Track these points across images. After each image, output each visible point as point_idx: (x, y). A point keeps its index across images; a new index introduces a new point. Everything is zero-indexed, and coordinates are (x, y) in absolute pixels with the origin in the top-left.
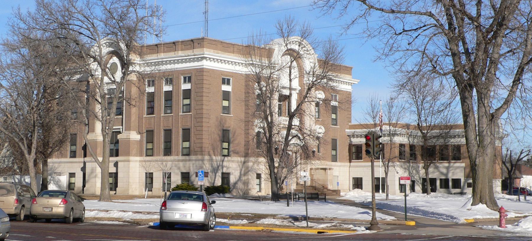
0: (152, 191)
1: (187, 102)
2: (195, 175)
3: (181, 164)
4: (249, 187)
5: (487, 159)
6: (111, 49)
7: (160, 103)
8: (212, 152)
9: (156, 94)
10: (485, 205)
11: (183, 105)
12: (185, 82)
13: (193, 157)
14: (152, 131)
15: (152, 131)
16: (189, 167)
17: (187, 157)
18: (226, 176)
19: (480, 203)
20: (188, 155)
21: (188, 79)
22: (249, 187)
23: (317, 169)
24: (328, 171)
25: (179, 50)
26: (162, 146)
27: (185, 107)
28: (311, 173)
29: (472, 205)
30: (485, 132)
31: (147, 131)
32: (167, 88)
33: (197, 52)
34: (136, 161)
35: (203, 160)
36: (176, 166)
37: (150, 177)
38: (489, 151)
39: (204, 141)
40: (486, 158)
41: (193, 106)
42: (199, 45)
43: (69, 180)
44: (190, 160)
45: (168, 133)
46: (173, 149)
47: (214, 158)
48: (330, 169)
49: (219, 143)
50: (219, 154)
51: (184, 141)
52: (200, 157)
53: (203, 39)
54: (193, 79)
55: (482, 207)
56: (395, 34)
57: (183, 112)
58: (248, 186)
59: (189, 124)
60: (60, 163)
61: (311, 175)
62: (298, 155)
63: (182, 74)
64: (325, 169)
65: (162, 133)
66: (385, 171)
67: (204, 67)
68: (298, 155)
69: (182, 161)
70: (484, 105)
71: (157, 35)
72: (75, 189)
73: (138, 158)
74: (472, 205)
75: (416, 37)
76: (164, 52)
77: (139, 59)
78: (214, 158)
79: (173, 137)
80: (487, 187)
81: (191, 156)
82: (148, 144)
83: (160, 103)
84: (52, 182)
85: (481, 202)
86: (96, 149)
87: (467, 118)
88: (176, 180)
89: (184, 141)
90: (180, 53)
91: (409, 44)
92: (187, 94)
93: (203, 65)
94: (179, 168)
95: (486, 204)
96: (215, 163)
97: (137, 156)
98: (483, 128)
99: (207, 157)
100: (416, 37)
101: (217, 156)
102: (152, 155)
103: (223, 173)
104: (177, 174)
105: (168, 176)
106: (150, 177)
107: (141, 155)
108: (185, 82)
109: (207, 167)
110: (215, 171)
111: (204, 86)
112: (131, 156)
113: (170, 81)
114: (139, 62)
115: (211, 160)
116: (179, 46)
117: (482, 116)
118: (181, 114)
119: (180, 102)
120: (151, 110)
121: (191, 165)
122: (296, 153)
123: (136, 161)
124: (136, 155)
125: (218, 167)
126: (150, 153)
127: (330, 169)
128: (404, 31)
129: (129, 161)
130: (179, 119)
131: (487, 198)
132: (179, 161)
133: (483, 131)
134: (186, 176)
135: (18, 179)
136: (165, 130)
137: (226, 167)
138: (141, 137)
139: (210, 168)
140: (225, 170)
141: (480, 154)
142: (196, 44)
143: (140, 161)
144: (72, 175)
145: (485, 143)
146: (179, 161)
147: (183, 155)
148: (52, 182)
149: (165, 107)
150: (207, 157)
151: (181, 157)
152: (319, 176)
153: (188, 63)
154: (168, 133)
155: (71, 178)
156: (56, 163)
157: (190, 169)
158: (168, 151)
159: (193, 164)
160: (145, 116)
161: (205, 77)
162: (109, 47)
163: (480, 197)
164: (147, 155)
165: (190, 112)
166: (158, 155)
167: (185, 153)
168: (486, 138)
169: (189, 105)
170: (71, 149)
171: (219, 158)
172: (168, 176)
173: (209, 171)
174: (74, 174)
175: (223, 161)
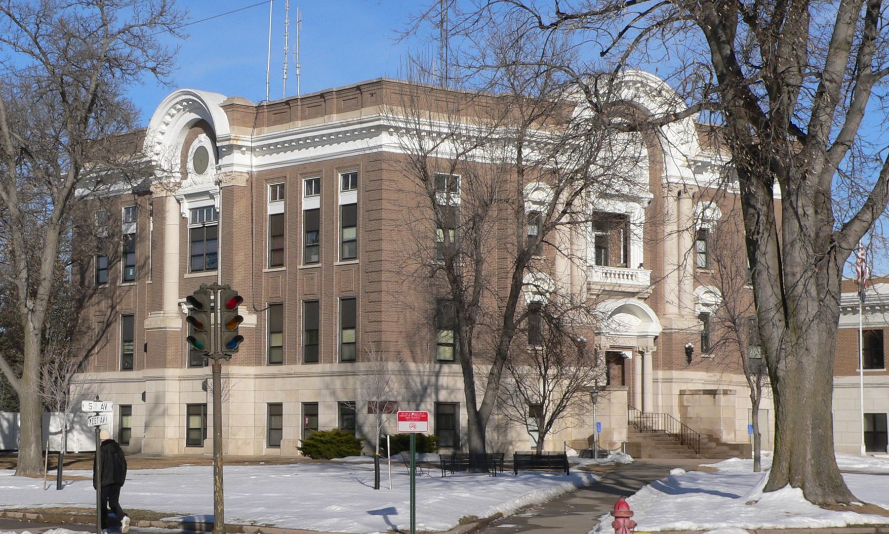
0: (278, 446)
1: (350, 234)
2: (365, 410)
3: (338, 383)
4: (509, 437)
5: (810, 364)
6: (194, 116)
7: (297, 237)
8: (406, 353)
9: (287, 216)
10: (799, 492)
11: (344, 242)
12: (345, 187)
13: (361, 366)
14: (281, 305)
15: (281, 305)
16: (355, 390)
17: (348, 364)
18: (448, 410)
19: (789, 485)
20: (352, 360)
21: (351, 182)
22: (509, 437)
23: (695, 392)
24: (722, 399)
25: (332, 113)
26: (301, 340)
27: (346, 247)
28: (681, 401)
29: (765, 491)
30: (800, 288)
31: (271, 305)
32: (311, 203)
33: (368, 113)
34: (247, 376)
35: (381, 372)
36: (327, 388)
37: (275, 410)
38: (815, 338)
39: (384, 326)
40: (804, 360)
41: (361, 242)
42: (374, 99)
43: (121, 422)
44: (354, 374)
45: (312, 306)
46: (322, 349)
47: (412, 366)
48: (725, 392)
49: (425, 333)
50: (426, 358)
51: (345, 327)
52: (374, 365)
53: (379, 83)
54: (361, 181)
55: (791, 495)
56: (541, 26)
57: (343, 259)
58: (506, 435)
59: (353, 287)
60: (102, 382)
61: (683, 408)
62: (649, 358)
63: (339, 169)
64: (713, 393)
65: (301, 310)
66: (752, 397)
67: (384, 149)
68: (649, 358)
69: (340, 374)
70: (796, 213)
71: (154, 70)
72: (131, 442)
73: (252, 370)
74: (765, 491)
75: (621, 34)
76: (303, 118)
77: (248, 137)
78: (412, 366)
79: (323, 318)
80: (809, 440)
81: (357, 364)
82: (273, 336)
83: (297, 237)
84: (77, 427)
85: (791, 481)
86: (165, 348)
87: (755, 250)
88: (329, 420)
89: (345, 327)
90: (335, 119)
91: (603, 54)
92: (350, 214)
93: (381, 146)
94: (333, 393)
95: (803, 488)
96: (418, 380)
97: (249, 364)
98: (794, 275)
99: (392, 366)
100: (621, 34)
101: (422, 361)
102: (280, 363)
103: (438, 404)
104: (329, 407)
105: (310, 410)
106: (275, 410)
107: (259, 363)
108: (345, 187)
109: (395, 389)
110: (417, 398)
111: (385, 195)
112: (234, 364)
113: (315, 187)
114: (249, 144)
115: (405, 372)
116: (334, 101)
117: (792, 244)
118: (338, 263)
119: (335, 233)
120: (277, 255)
121: (358, 386)
122: (642, 353)
123: (247, 376)
124: (247, 363)
125: (425, 389)
126: (275, 357)
127: (725, 392)
128: (564, 17)
129: (163, 379)
130: (332, 276)
131: (809, 469)
132: (332, 374)
133: (795, 285)
134: (347, 411)
135: (8, 420)
136: (342, 300)
137: (447, 388)
138: (259, 319)
139: (403, 390)
140: (443, 396)
141: (789, 349)
142: (366, 95)
143: (257, 377)
144: (126, 410)
145: (802, 317)
146: (332, 374)
147: (343, 361)
148: (77, 427)
149: (307, 247)
150: (392, 366)
151: (337, 367)
152: (700, 408)
153: (351, 143)
154: (312, 306)
155: (125, 418)
156: (92, 382)
157: (355, 397)
158: (311, 356)
159: (362, 383)
160: (267, 270)
161: (385, 175)
162: (190, 111)
163: (790, 469)
164: (271, 363)
165: (355, 258)
166: (293, 362)
167: (346, 357)
168: (803, 303)
169: (354, 241)
170: (123, 350)
171: (426, 367)
172: (310, 410)
173: (399, 398)
174: (130, 407)
175: (437, 374)
